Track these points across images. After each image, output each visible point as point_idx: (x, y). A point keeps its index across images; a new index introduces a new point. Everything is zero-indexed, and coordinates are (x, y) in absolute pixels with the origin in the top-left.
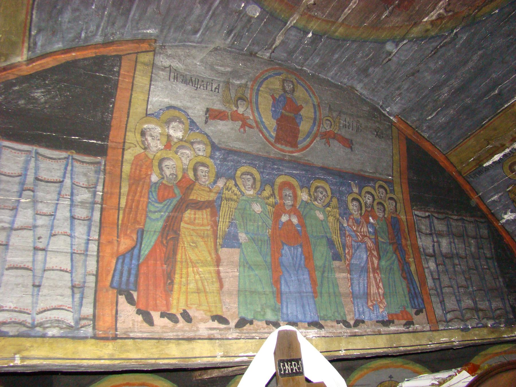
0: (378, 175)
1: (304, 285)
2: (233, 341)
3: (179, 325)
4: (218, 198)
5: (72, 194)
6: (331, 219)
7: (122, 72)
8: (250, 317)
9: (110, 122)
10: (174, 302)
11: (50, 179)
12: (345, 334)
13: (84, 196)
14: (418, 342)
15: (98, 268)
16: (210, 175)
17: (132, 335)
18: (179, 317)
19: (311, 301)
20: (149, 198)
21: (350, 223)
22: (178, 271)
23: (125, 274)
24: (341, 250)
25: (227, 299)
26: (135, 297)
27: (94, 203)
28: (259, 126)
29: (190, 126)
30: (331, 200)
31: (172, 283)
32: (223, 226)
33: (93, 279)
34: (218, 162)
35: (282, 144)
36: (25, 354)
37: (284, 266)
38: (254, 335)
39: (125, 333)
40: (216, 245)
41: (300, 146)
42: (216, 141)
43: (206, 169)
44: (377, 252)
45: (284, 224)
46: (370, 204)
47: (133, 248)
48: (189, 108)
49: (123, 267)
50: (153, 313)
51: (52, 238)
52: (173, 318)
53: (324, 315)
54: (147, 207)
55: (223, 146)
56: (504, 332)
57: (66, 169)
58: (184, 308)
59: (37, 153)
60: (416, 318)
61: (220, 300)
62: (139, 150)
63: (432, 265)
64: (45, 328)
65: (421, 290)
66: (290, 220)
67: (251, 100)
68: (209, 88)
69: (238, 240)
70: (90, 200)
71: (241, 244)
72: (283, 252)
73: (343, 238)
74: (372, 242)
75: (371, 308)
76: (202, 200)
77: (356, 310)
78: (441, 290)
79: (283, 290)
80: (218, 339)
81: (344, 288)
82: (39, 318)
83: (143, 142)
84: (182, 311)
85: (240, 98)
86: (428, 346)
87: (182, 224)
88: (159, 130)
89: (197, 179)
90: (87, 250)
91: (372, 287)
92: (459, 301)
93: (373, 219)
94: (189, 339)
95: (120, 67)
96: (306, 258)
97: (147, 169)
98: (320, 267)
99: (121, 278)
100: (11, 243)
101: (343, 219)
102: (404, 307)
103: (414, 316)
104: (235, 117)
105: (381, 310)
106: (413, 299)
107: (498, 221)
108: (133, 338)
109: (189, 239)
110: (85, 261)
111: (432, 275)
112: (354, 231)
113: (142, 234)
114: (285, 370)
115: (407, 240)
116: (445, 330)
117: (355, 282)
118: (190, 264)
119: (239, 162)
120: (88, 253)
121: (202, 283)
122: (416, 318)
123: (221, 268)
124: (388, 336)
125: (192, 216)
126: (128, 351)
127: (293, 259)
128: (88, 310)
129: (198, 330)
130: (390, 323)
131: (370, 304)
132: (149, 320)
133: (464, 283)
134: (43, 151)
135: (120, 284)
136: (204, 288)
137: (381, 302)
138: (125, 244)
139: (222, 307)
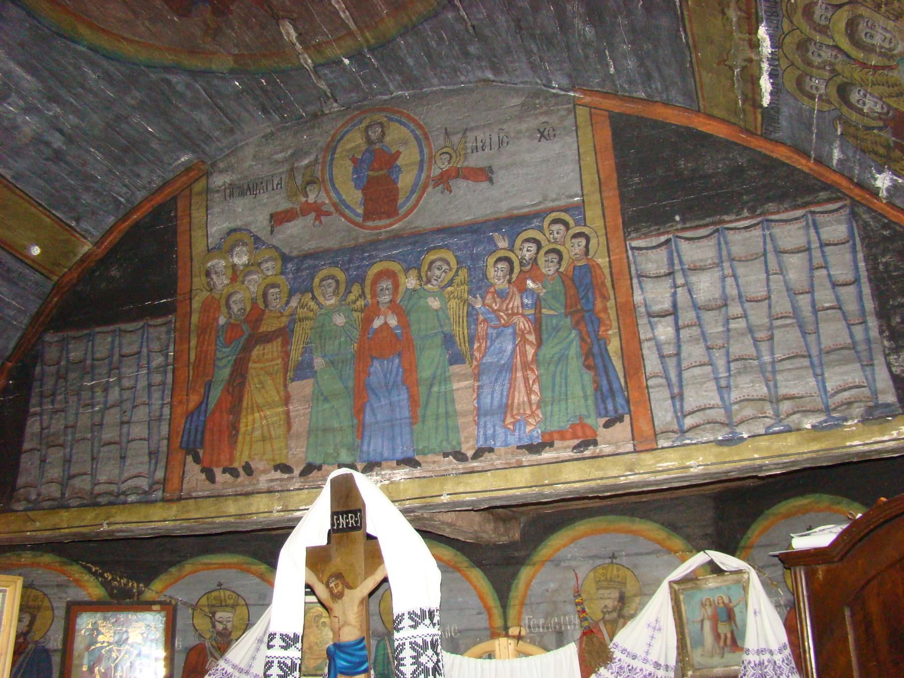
0: (550, 205)
1: (398, 409)
3: (239, 480)
4: (290, 322)
5: (148, 363)
6: (453, 303)
7: (179, 214)
8: (318, 462)
9: (176, 274)
11: (132, 352)
12: (454, 472)
13: (158, 360)
14: (600, 474)
15: (169, 432)
16: (282, 295)
17: (194, 494)
18: (241, 471)
19: (406, 430)
20: (216, 344)
21: (489, 299)
22: (243, 420)
23: (193, 432)
24: (464, 348)
26: (201, 455)
27: (167, 365)
28: (340, 207)
29: (255, 243)
30: (456, 274)
32: (295, 355)
33: (165, 442)
34: (291, 276)
35: (374, 220)
36: (112, 520)
37: (373, 390)
39: (188, 494)
40: (285, 380)
41: (402, 211)
42: (286, 251)
43: (277, 290)
44: (536, 334)
45: (376, 331)
46: (530, 259)
47: (201, 403)
48: (250, 224)
49: (191, 425)
50: (215, 469)
51: (135, 410)
52: (234, 473)
53: (424, 447)
54: (215, 354)
55: (295, 253)
56: (852, 436)
57: (143, 337)
58: (246, 460)
59: (120, 331)
62: (206, 294)
64: (127, 495)
65: (626, 382)
66: (386, 323)
67: (323, 179)
68: (270, 188)
70: (164, 363)
72: (372, 370)
73: (473, 327)
75: (511, 427)
76: (273, 329)
77: (482, 433)
78: (680, 375)
79: (366, 421)
80: (278, 491)
82: (124, 487)
83: (208, 283)
84: (244, 464)
85: (308, 183)
86: (622, 478)
87: (251, 365)
88: (223, 263)
89: (266, 306)
90: (161, 415)
91: (516, 394)
93: (534, 282)
94: (247, 494)
95: (176, 210)
96: (405, 371)
97: (214, 313)
98: (427, 380)
99: (189, 437)
100: (104, 422)
101: (476, 298)
102: (581, 418)
103: (601, 431)
104: (306, 210)
105: (529, 428)
106: (604, 402)
108: (195, 498)
112: (494, 311)
113: (210, 387)
114: (338, 525)
115: (608, 299)
118: (255, 409)
119: (315, 267)
121: (269, 428)
123: (291, 408)
125: (261, 352)
126: (188, 512)
127: (385, 376)
131: (509, 420)
132: (211, 478)
134: (124, 326)
135: (188, 444)
136: (270, 435)
138: (194, 399)
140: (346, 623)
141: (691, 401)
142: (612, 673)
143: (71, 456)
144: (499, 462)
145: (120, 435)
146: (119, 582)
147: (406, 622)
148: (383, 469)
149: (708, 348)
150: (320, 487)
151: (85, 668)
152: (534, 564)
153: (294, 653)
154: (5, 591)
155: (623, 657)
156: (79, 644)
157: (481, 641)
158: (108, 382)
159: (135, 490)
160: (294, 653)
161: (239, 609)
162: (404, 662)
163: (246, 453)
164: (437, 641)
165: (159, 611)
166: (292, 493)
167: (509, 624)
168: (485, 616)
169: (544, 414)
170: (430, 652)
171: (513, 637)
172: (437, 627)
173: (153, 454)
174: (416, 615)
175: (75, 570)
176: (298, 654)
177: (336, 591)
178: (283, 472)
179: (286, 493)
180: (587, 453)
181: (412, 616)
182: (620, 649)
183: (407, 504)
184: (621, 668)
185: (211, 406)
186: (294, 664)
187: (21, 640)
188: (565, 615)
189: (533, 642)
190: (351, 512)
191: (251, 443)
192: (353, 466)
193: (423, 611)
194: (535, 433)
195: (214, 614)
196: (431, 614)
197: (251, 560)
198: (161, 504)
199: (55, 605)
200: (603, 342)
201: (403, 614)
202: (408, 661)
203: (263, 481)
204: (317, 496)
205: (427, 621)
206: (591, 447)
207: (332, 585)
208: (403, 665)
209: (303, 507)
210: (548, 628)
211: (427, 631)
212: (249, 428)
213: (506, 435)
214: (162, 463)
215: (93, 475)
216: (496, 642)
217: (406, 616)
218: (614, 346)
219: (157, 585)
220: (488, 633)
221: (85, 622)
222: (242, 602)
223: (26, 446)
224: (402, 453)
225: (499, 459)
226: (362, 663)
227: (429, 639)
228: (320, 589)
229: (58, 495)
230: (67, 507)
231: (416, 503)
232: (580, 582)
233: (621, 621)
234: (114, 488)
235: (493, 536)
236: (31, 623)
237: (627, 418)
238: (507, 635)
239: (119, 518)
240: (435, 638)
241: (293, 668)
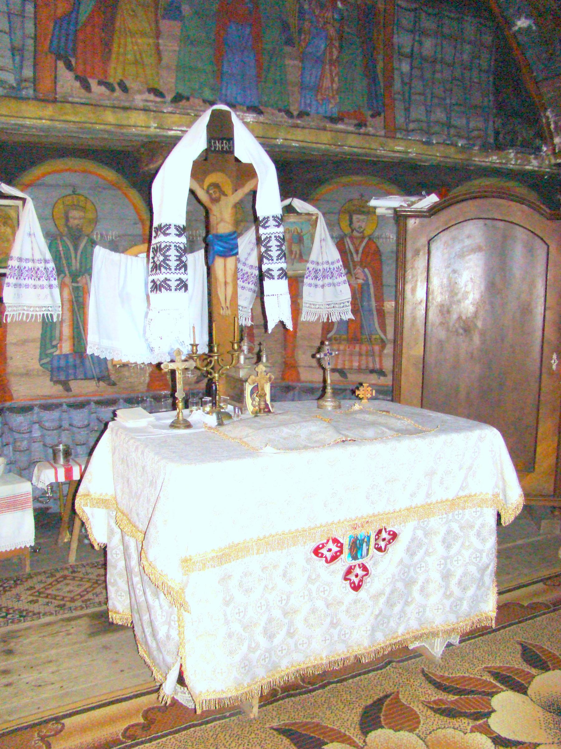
2: (168, 115)
8: (186, 94)
10: (112, 72)
14: (367, 146)
17: (70, 99)
22: (116, 41)
25: (164, 73)
31: (110, 52)
33: (30, 42)
38: (189, 111)
39: (64, 97)
52: (110, 87)
56: (475, 156)
58: (120, 78)
60: (370, 121)
61: (158, 75)
63: (405, 67)
69: (180, 12)
71: (184, 17)
74: (336, 30)
78: (410, 97)
80: (154, 111)
81: (293, 76)
84: (118, 80)
92: (428, 112)
94: (125, 109)
102: (359, 108)
105: (331, 106)
107: (510, 28)
108: (72, 103)
109: (128, 7)
110: (23, 22)
111: (402, 78)
112: (316, 16)
116: (402, 139)
117: (307, 73)
118: (128, 34)
120: (26, 15)
122: (370, 121)
123: (161, 41)
124: (333, 134)
126: (65, 114)
128: (28, 73)
129: (134, 100)
131: (319, 97)
132: (87, 87)
133: (441, 94)
137: (333, 97)
139: (159, 80)
140: (222, 220)
141: (414, 115)
149: (424, 86)
162: (276, 248)
163: (120, 71)
166: (165, 115)
168: (140, 226)
169: (340, 98)
174: (278, 218)
178: (156, 95)
179: (160, 114)
185: (82, 18)
190: (224, 139)
194: (334, 110)
200: (374, 62)
203: (139, 99)
206: (364, 128)
207: (211, 192)
218: (380, 66)
226: (232, 250)
237: (383, 115)
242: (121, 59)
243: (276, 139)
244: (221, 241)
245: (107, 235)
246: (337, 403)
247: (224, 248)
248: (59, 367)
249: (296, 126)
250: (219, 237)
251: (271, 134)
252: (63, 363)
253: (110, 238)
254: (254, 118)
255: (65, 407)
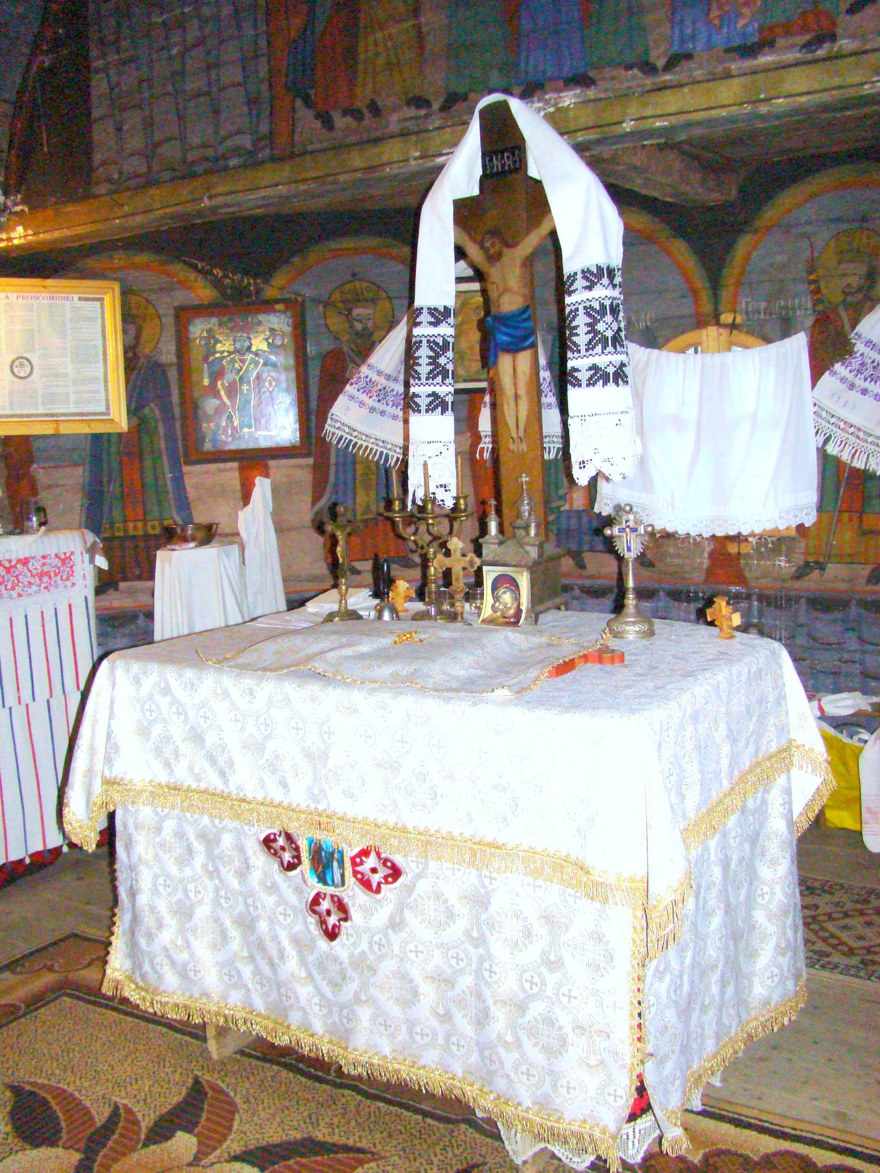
3: (366, 122)
8: (461, 90)
14: (837, 81)
17: (309, 148)
22: (362, 43)
36: (213, 192)
52: (357, 115)
75: (717, 22)
82: (222, 149)
86: (866, 87)
94: (377, 141)
108: (312, 152)
114: (492, 168)
130: (764, 46)
131: (714, 13)
138: (297, 22)
140: (506, 290)
142: (851, 371)
143: (152, 117)
144: (700, 72)
145: (209, 84)
146: (233, 279)
147: (580, 283)
148: (546, 93)
150: (466, 124)
151: (206, 382)
152: (756, 232)
153: (446, 330)
154: (102, 300)
155: (866, 350)
156: (196, 354)
157: (684, 332)
158: (183, 14)
159: (236, 151)
160: (446, 330)
161: (380, 303)
162: (578, 331)
163: (370, 87)
164: (618, 305)
165: (284, 312)
167: (721, 309)
168: (690, 300)
170: (609, 318)
171: (725, 326)
172: (618, 290)
173: (252, 102)
174: (592, 273)
175: (179, 270)
176: (450, 331)
177: (492, 251)
178: (418, 107)
180: (820, 53)
181: (586, 274)
182: (863, 340)
183: (580, 137)
184: (863, 364)
186: (446, 344)
187: (130, 355)
188: (794, 297)
189: (751, 332)
190: (506, 150)
191: (375, 74)
192: (508, 91)
193: (599, 268)
195: (350, 311)
196: (611, 273)
197: (389, 241)
198: (269, 165)
199: (161, 312)
201: (576, 274)
202: (582, 330)
203: (394, 122)
204: (464, 132)
205: (605, 281)
207: (488, 245)
208: (577, 335)
209: (448, 151)
210: (771, 314)
211: (602, 293)
212: (371, 54)
213: (710, 35)
214: (265, 114)
215: (183, 138)
216: (704, 332)
217: (579, 276)
219: (279, 279)
220: (695, 321)
221: (198, 329)
222: (385, 295)
223: (96, 113)
224: (571, 68)
225: (699, 69)
226: (526, 338)
227: (607, 303)
228: (473, 251)
229: (143, 169)
230: (156, 183)
231: (592, 136)
232: (816, 254)
233: (869, 303)
234: (210, 152)
235: (700, 191)
236: (138, 337)
238: (718, 323)
239: (220, 189)
240: (615, 302)
241: (445, 347)
242: (371, 67)
243: (621, 122)
244: (507, 326)
245: (638, 321)
246: (646, 627)
247: (512, 336)
248: (568, 530)
249: (662, 88)
250: (503, 320)
251: (607, 118)
252: (573, 523)
253: (642, 325)
254: (575, 96)
255: (577, 592)
